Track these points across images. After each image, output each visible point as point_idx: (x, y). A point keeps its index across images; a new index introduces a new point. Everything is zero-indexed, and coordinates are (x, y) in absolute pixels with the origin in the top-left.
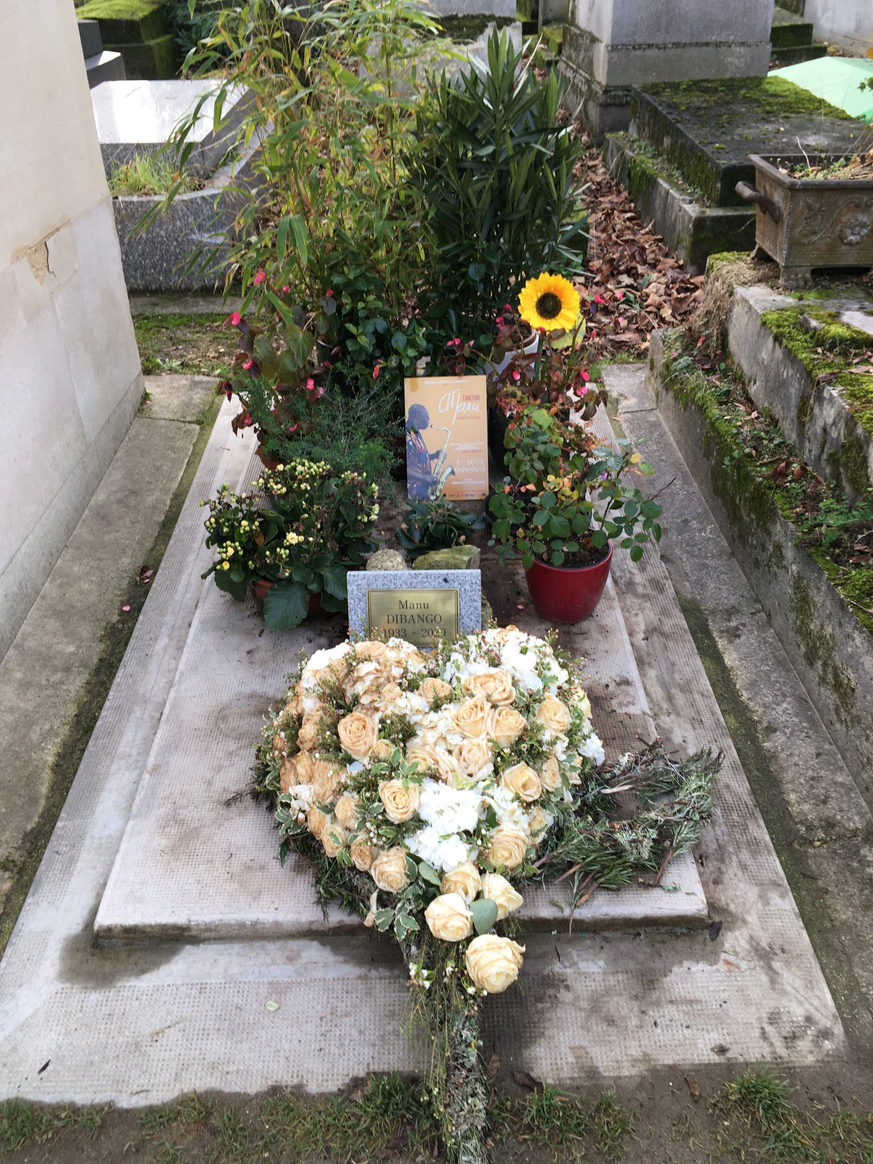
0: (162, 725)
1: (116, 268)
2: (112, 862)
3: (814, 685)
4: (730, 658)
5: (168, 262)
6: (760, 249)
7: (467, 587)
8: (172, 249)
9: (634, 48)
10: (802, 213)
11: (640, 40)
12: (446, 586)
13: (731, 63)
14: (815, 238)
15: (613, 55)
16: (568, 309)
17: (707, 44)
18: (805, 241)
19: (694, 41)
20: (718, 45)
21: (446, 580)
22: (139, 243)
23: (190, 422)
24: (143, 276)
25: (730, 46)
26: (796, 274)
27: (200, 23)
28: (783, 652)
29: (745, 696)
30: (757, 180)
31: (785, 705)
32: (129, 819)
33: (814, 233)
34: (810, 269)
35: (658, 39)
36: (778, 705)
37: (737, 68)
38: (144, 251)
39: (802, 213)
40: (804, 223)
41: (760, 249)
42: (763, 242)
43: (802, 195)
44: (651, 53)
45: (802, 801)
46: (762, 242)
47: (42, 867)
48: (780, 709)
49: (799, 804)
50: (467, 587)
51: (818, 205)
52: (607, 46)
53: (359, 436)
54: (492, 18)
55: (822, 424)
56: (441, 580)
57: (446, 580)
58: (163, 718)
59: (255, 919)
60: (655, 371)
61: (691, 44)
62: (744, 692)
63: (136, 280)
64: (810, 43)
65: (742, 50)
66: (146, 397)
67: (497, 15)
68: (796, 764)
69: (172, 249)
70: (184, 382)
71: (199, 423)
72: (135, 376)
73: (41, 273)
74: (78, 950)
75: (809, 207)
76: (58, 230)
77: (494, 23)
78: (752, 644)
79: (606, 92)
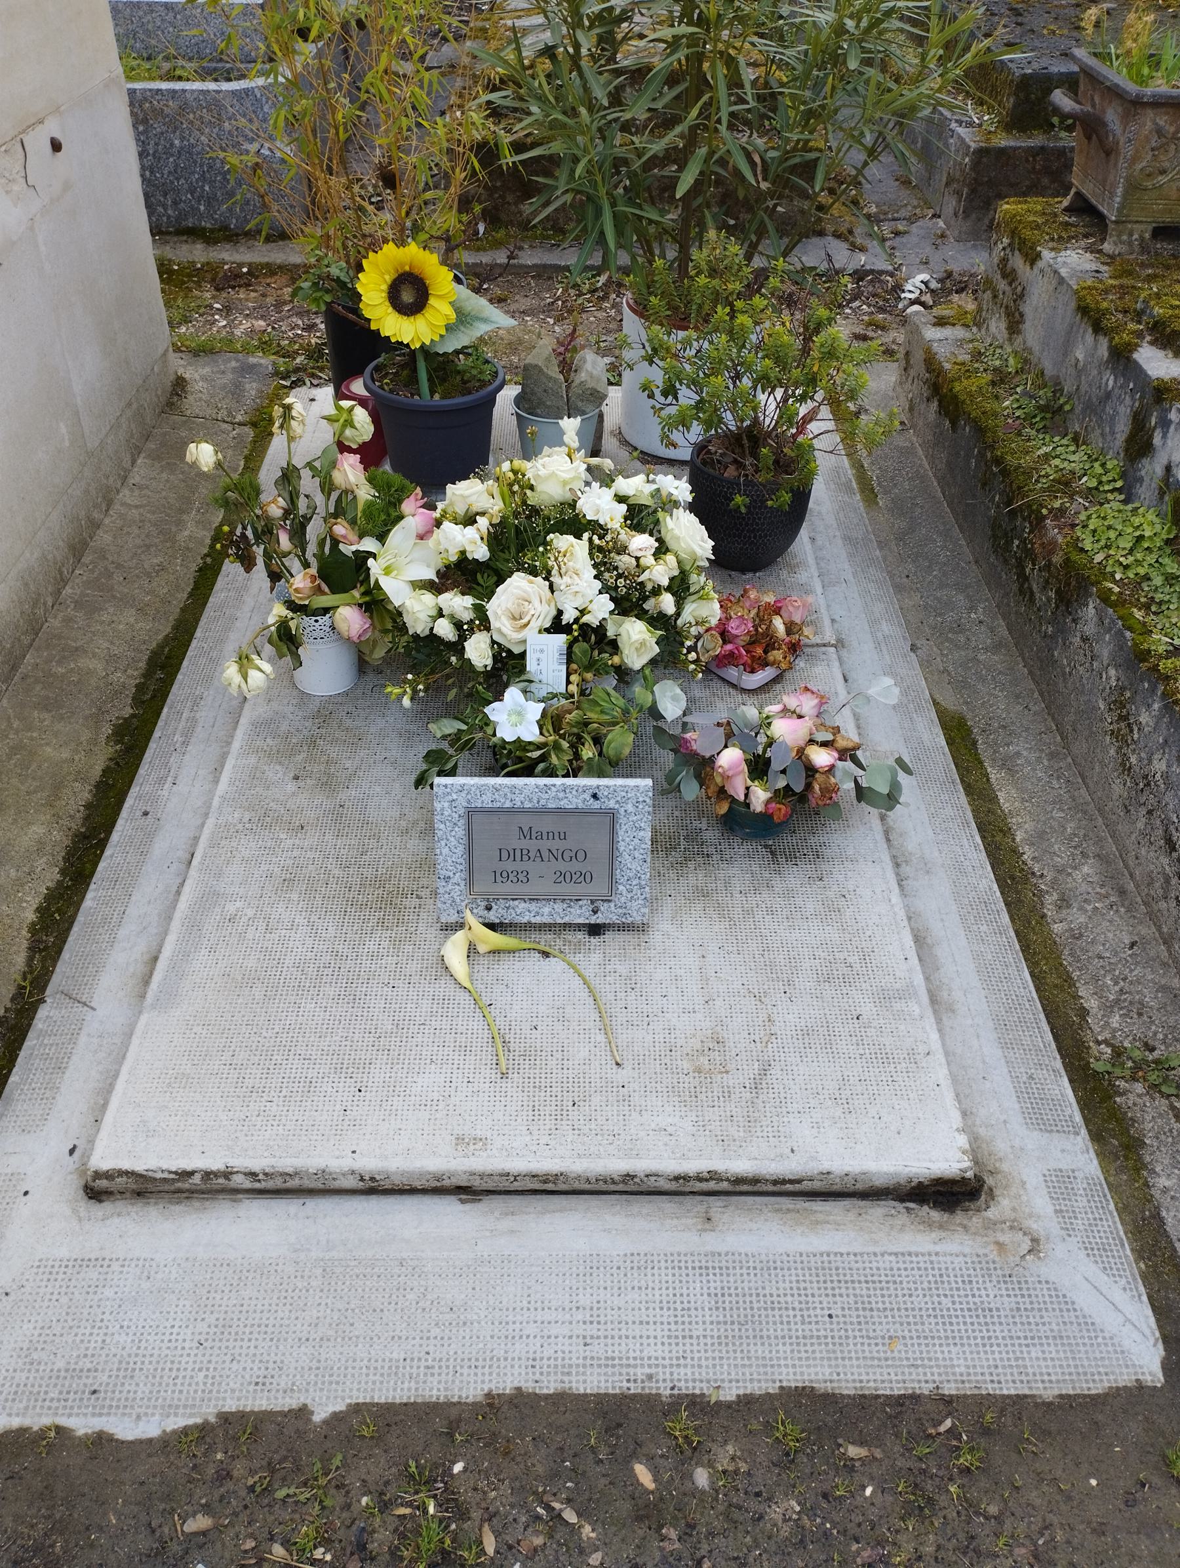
0: (193, 872)
1: (133, 186)
2: (116, 1076)
3: (1130, 842)
4: (1007, 798)
5: (212, 183)
6: (1078, 194)
10: (1148, 140)
14: (1162, 179)
16: (439, 297)
18: (1149, 184)
21: (595, 796)
22: (168, 154)
23: (240, 424)
24: (175, 203)
26: (1131, 235)
28: (1083, 791)
29: (1028, 853)
30: (1082, 87)
31: (1086, 869)
32: (140, 1012)
33: (1163, 172)
34: (1150, 228)
36: (1075, 868)
38: (177, 165)
39: (1148, 140)
40: (1149, 157)
41: (1078, 194)
42: (1083, 182)
43: (1150, 113)
45: (1109, 1008)
46: (1078, 181)
47: (13, 1078)
48: (1077, 875)
49: (1107, 1026)
51: (1172, 129)
55: (1165, 462)
56: (587, 796)
57: (595, 796)
58: (195, 862)
59: (322, 1165)
60: (912, 372)
62: (1026, 848)
66: (180, 385)
68: (1100, 957)
70: (234, 364)
71: (254, 425)
72: (161, 351)
73: (16, 188)
75: (1159, 132)
76: (41, 122)
78: (1039, 779)
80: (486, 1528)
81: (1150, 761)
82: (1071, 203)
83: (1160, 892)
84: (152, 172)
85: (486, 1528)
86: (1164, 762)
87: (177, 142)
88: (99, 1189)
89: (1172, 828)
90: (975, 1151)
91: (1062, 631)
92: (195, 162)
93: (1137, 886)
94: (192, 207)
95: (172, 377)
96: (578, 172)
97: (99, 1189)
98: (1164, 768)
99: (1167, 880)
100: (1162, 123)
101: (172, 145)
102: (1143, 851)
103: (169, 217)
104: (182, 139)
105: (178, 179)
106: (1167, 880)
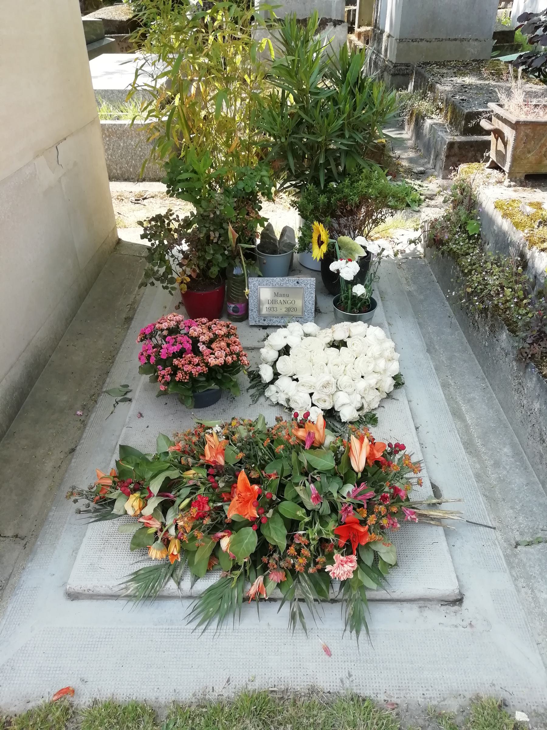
5: (135, 160)
7: (308, 286)
8: (138, 153)
9: (412, 41)
11: (416, 36)
12: (298, 286)
13: (469, 51)
15: (400, 44)
17: (455, 40)
19: (448, 38)
20: (462, 40)
21: (298, 282)
24: (120, 168)
25: (469, 41)
27: (278, 32)
35: (427, 37)
37: (472, 54)
38: (121, 153)
39: (522, 139)
44: (423, 44)
50: (308, 286)
52: (396, 39)
53: (231, 197)
54: (331, 20)
56: (295, 282)
57: (298, 282)
61: (446, 40)
63: (117, 171)
64: (513, 41)
65: (476, 43)
67: (333, 19)
69: (138, 153)
74: (157, 699)
77: (332, 23)
79: (395, 67)
80: (353, 437)
81: (532, 403)
82: (490, 165)
83: (538, 461)
84: (111, 156)
85: (353, 437)
86: (538, 403)
87: (122, 144)
88: (73, 596)
89: (543, 433)
90: (461, 586)
91: (492, 346)
92: (129, 152)
93: (528, 458)
94: (127, 170)
95: (114, 240)
96: (434, 150)
97: (73, 596)
98: (539, 406)
99: (541, 456)
100: (528, 132)
101: (120, 145)
102: (530, 443)
103: (118, 174)
104: (124, 143)
105: (122, 159)
106: (541, 456)
